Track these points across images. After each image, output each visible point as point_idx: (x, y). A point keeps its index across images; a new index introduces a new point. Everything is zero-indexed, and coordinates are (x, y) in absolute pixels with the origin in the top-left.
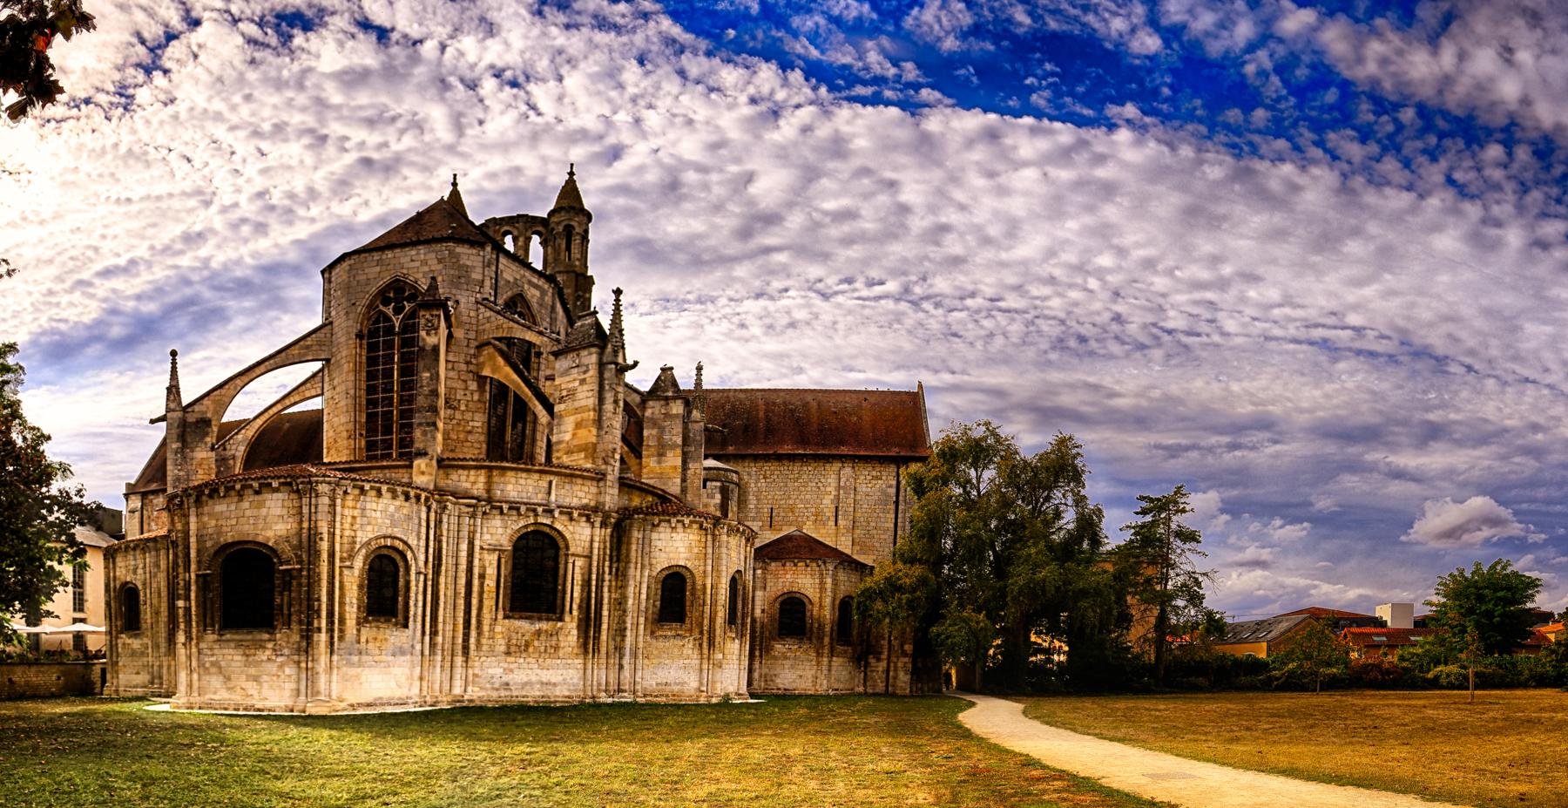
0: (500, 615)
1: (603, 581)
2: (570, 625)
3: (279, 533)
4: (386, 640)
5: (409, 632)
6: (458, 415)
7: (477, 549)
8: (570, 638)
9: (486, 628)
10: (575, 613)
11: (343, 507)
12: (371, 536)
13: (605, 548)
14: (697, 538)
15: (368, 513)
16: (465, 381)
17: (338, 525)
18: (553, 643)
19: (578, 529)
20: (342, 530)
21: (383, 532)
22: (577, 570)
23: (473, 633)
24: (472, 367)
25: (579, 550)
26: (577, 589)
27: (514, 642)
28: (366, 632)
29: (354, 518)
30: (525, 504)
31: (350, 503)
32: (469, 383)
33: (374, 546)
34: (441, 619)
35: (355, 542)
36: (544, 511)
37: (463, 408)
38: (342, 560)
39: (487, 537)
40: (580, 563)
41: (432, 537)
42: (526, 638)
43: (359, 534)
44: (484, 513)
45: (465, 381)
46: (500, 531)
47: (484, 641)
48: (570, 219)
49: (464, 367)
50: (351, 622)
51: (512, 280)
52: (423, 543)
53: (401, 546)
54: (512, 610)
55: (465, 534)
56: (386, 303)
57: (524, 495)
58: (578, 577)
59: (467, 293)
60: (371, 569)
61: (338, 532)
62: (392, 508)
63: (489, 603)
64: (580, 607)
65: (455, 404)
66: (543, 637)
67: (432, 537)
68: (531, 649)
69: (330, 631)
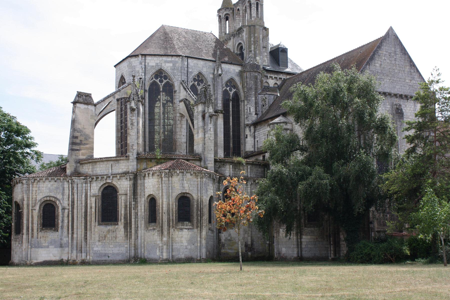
2: (121, 226)
4: (47, 237)
7: (89, 196)
8: (121, 233)
9: (93, 230)
11: (33, 187)
12: (42, 197)
15: (40, 188)
18: (115, 235)
19: (122, 183)
20: (32, 196)
26: (123, 210)
28: (40, 234)
29: (36, 191)
30: (100, 175)
31: (35, 186)
33: (43, 200)
34: (75, 227)
35: (36, 200)
38: (33, 207)
40: (123, 197)
43: (38, 197)
50: (35, 231)
51: (154, 64)
52: (66, 197)
53: (53, 199)
55: (84, 191)
57: (102, 171)
62: (49, 185)
63: (93, 219)
64: (125, 218)
66: (111, 233)
67: (70, 194)
68: (106, 239)
69: (28, 234)
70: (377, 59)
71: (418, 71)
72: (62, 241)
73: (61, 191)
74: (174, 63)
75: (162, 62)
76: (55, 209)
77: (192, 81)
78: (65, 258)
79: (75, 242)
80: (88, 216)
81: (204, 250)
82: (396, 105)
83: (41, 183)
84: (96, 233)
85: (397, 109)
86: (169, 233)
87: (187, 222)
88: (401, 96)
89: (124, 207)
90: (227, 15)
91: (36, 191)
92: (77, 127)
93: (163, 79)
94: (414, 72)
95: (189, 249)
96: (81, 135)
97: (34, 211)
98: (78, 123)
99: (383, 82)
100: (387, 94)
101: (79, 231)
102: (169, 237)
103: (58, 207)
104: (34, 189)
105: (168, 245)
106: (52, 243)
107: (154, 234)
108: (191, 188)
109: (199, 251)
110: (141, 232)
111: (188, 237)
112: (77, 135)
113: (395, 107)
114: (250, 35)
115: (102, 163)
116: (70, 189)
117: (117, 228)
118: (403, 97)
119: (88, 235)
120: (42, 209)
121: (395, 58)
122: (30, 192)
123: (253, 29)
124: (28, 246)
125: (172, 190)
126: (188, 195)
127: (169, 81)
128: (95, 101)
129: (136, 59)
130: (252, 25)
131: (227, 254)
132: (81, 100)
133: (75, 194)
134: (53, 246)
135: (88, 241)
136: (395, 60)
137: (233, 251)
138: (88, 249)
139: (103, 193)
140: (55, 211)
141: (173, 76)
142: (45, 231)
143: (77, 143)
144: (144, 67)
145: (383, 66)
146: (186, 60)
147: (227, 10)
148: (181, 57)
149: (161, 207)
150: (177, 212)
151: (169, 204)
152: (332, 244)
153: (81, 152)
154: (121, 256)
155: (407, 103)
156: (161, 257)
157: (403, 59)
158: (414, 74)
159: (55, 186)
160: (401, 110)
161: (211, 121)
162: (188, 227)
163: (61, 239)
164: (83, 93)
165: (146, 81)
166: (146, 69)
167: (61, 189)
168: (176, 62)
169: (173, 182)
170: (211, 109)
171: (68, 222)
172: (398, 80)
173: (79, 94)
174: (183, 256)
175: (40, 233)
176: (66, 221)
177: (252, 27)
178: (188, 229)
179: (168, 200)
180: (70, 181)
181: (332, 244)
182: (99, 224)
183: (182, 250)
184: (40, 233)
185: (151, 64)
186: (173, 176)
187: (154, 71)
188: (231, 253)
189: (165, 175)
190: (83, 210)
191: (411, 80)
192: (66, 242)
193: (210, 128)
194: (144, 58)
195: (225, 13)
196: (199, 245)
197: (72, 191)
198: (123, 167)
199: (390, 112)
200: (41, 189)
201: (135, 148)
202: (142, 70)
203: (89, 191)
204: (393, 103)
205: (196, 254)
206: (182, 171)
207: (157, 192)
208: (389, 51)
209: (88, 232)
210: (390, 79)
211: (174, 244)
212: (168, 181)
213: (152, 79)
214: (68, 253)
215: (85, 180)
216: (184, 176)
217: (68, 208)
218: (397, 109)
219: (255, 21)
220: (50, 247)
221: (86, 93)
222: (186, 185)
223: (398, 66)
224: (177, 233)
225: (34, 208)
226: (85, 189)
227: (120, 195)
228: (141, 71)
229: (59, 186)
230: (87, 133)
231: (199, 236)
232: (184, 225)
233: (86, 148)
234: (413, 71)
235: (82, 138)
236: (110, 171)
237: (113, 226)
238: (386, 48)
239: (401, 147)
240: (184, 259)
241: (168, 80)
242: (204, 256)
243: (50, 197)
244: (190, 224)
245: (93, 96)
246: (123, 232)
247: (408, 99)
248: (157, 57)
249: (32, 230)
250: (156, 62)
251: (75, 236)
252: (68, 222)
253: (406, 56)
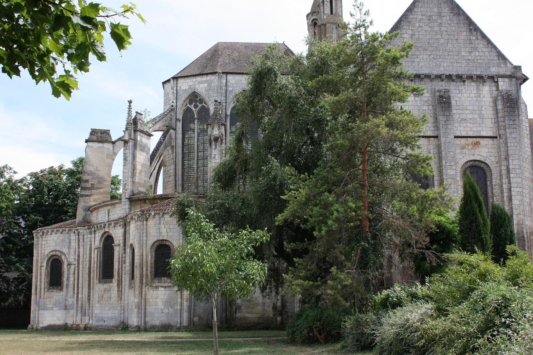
4: (52, 297)
7: (93, 248)
12: (49, 251)
29: (45, 245)
31: (44, 239)
33: (49, 256)
34: (80, 286)
70: (405, 27)
71: (484, 36)
72: (67, 302)
73: (68, 244)
74: (209, 83)
75: (196, 84)
77: (234, 102)
78: (70, 322)
79: (80, 303)
81: (185, 315)
82: (439, 91)
85: (441, 97)
87: (166, 278)
88: (449, 77)
90: (315, 21)
92: (88, 170)
93: (198, 103)
94: (477, 39)
95: (166, 313)
96: (93, 178)
98: (90, 165)
99: (418, 60)
100: (422, 76)
102: (142, 297)
103: (64, 263)
104: (44, 243)
105: (140, 308)
106: (57, 304)
108: (170, 234)
109: (179, 316)
111: (165, 298)
112: (87, 179)
113: (438, 94)
114: (321, 36)
117: (111, 287)
118: (454, 78)
121: (440, 22)
123: (324, 28)
125: (147, 236)
126: (167, 243)
127: (205, 105)
128: (114, 139)
130: (322, 24)
131: (245, 319)
132: (94, 138)
134: (57, 308)
136: (440, 25)
137: (254, 316)
141: (207, 98)
142: (51, 291)
143: (88, 188)
145: (417, 36)
146: (225, 77)
147: (314, 14)
148: (217, 74)
150: (153, 265)
151: (143, 255)
153: (92, 198)
154: (114, 320)
155: (463, 87)
157: (455, 22)
158: (477, 42)
159: (61, 238)
160: (449, 97)
161: (216, 146)
162: (167, 285)
163: (66, 300)
164: (98, 130)
165: (178, 109)
166: (178, 95)
167: (68, 241)
168: (211, 82)
169: (148, 227)
170: (216, 131)
171: (74, 280)
172: (446, 53)
173: (93, 131)
174: (157, 323)
175: (46, 293)
176: (72, 279)
177: (322, 27)
178: (166, 287)
179: (141, 250)
182: (100, 282)
183: (156, 315)
184: (46, 293)
185: (184, 87)
186: (149, 220)
187: (187, 95)
188: (251, 318)
191: (470, 53)
192: (71, 303)
193: (215, 155)
195: (312, 19)
196: (179, 307)
198: (118, 212)
199: (430, 103)
201: (127, 188)
203: (93, 243)
204: (435, 89)
205: (175, 321)
206: (158, 212)
208: (429, 14)
209: (91, 291)
210: (429, 53)
211: (148, 307)
212: (142, 226)
213: (186, 105)
214: (73, 316)
215: (90, 230)
216: (161, 219)
217: (74, 263)
218: (441, 97)
219: (327, 18)
220: (54, 309)
221: (103, 130)
222: (164, 230)
223: (445, 33)
224: (152, 292)
227: (115, 245)
229: (65, 238)
230: (101, 175)
231: (180, 296)
232: (161, 282)
233: (100, 192)
234: (474, 38)
235: (95, 182)
236: (107, 218)
238: (423, 9)
239: (446, 154)
240: (159, 326)
241: (203, 104)
242: (185, 323)
243: (56, 251)
244: (169, 281)
245: (111, 133)
247: (464, 81)
248: (190, 78)
249: (41, 289)
250: (189, 84)
251: (80, 296)
252: (74, 280)
253: (462, 18)
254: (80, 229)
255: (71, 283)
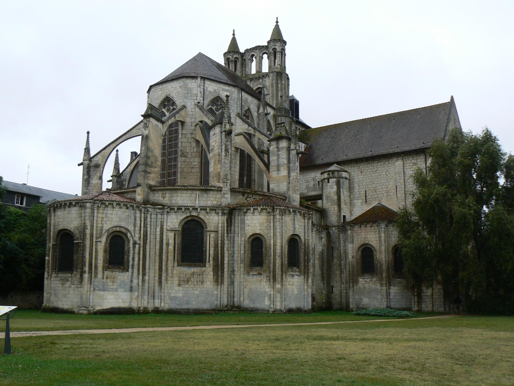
0: (176, 265)
1: (224, 244)
2: (209, 269)
3: (75, 226)
5: (129, 274)
6: (187, 160)
7: (165, 230)
8: (209, 277)
9: (170, 272)
10: (211, 262)
11: (98, 213)
13: (224, 227)
14: (266, 217)
15: (109, 215)
16: (190, 143)
17: (95, 222)
18: (201, 279)
19: (211, 217)
20: (97, 224)
21: (116, 224)
22: (212, 239)
23: (164, 275)
24: (193, 136)
25: (212, 229)
26: (212, 249)
27: (182, 279)
29: (102, 218)
31: (101, 211)
32: (192, 143)
33: (111, 231)
34: (147, 267)
35: (102, 230)
36: (193, 209)
37: (190, 156)
38: (97, 238)
39: (169, 224)
40: (213, 235)
41: (142, 225)
42: (187, 276)
43: (104, 225)
44: (168, 212)
45: (190, 143)
46: (175, 220)
47: (169, 279)
48: (275, 45)
49: (190, 136)
50: (100, 268)
51: (212, 90)
52: (137, 228)
53: (124, 231)
54: (183, 261)
55: (159, 223)
56: (165, 106)
57: (185, 202)
58: (212, 243)
59: (191, 101)
60: (110, 243)
61: (95, 225)
63: (171, 258)
64: (214, 259)
65: (186, 154)
66: (195, 276)
67: (142, 225)
68: (190, 283)
69: (90, 272)
73: (133, 221)
76: (124, 243)
78: (134, 305)
80: (164, 254)
83: (109, 209)
84: (175, 276)
86: (282, 279)
87: (296, 268)
89: (213, 246)
90: (236, 59)
91: (102, 218)
97: (99, 244)
98: (151, 141)
101: (152, 271)
103: (129, 241)
104: (100, 215)
107: (261, 280)
110: (240, 276)
115: (185, 192)
116: (143, 219)
119: (163, 278)
120: (109, 241)
122: (95, 219)
124: (90, 288)
129: (194, 81)
133: (148, 226)
135: (163, 285)
138: (163, 295)
139: (183, 228)
140: (124, 245)
144: (203, 91)
149: (272, 248)
152: (416, 296)
156: (272, 306)
159: (127, 214)
167: (133, 218)
175: (106, 272)
176: (136, 259)
180: (143, 210)
181: (416, 296)
187: (212, 97)
189: (279, 213)
190: (158, 247)
194: (202, 82)
197: (144, 223)
200: (109, 216)
202: (201, 93)
207: (266, 232)
220: (119, 290)
225: (99, 240)
226: (160, 221)
227: (209, 231)
228: (199, 95)
229: (131, 214)
232: (293, 271)
237: (199, 268)
243: (120, 227)
246: (212, 276)
254: (150, 208)
255: (136, 263)
